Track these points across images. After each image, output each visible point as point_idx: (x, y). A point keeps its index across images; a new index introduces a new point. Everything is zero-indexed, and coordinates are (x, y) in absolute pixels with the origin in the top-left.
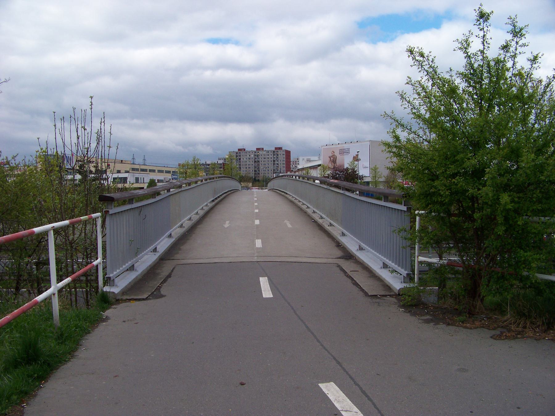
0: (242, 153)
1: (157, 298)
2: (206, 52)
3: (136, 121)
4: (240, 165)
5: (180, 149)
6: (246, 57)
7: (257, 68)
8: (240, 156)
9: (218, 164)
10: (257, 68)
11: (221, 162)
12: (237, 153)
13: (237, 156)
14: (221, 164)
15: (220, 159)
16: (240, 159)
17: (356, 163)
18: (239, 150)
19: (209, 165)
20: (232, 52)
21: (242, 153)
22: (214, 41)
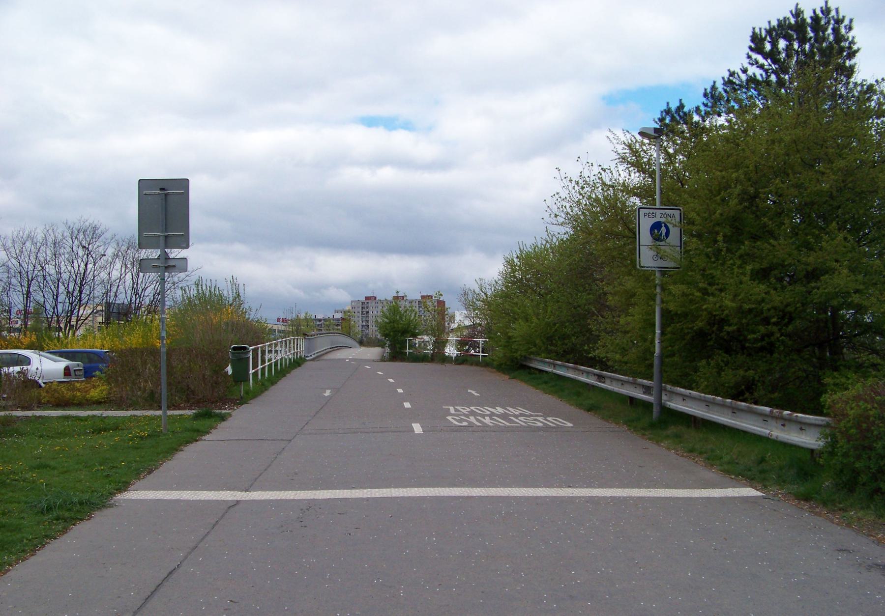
0: (372, 304)
1: (34, 551)
2: (361, 139)
3: (239, 247)
4: (367, 321)
5: (299, 294)
6: (424, 149)
7: (441, 165)
8: (368, 307)
9: (334, 319)
10: (441, 165)
11: (338, 316)
12: (363, 303)
13: (363, 308)
14: (338, 320)
15: (336, 312)
16: (368, 312)
17: (315, 332)
18: (367, 298)
19: (320, 320)
20: (401, 141)
21: (372, 304)
22: (370, 122)
